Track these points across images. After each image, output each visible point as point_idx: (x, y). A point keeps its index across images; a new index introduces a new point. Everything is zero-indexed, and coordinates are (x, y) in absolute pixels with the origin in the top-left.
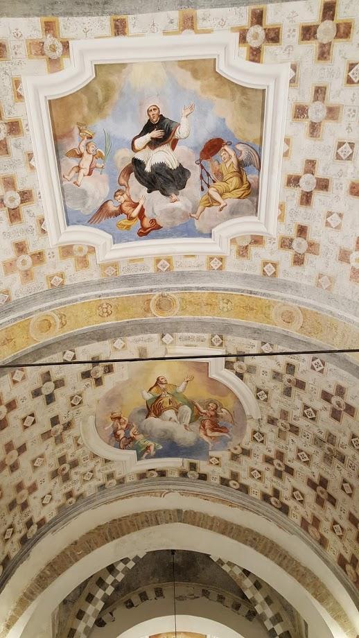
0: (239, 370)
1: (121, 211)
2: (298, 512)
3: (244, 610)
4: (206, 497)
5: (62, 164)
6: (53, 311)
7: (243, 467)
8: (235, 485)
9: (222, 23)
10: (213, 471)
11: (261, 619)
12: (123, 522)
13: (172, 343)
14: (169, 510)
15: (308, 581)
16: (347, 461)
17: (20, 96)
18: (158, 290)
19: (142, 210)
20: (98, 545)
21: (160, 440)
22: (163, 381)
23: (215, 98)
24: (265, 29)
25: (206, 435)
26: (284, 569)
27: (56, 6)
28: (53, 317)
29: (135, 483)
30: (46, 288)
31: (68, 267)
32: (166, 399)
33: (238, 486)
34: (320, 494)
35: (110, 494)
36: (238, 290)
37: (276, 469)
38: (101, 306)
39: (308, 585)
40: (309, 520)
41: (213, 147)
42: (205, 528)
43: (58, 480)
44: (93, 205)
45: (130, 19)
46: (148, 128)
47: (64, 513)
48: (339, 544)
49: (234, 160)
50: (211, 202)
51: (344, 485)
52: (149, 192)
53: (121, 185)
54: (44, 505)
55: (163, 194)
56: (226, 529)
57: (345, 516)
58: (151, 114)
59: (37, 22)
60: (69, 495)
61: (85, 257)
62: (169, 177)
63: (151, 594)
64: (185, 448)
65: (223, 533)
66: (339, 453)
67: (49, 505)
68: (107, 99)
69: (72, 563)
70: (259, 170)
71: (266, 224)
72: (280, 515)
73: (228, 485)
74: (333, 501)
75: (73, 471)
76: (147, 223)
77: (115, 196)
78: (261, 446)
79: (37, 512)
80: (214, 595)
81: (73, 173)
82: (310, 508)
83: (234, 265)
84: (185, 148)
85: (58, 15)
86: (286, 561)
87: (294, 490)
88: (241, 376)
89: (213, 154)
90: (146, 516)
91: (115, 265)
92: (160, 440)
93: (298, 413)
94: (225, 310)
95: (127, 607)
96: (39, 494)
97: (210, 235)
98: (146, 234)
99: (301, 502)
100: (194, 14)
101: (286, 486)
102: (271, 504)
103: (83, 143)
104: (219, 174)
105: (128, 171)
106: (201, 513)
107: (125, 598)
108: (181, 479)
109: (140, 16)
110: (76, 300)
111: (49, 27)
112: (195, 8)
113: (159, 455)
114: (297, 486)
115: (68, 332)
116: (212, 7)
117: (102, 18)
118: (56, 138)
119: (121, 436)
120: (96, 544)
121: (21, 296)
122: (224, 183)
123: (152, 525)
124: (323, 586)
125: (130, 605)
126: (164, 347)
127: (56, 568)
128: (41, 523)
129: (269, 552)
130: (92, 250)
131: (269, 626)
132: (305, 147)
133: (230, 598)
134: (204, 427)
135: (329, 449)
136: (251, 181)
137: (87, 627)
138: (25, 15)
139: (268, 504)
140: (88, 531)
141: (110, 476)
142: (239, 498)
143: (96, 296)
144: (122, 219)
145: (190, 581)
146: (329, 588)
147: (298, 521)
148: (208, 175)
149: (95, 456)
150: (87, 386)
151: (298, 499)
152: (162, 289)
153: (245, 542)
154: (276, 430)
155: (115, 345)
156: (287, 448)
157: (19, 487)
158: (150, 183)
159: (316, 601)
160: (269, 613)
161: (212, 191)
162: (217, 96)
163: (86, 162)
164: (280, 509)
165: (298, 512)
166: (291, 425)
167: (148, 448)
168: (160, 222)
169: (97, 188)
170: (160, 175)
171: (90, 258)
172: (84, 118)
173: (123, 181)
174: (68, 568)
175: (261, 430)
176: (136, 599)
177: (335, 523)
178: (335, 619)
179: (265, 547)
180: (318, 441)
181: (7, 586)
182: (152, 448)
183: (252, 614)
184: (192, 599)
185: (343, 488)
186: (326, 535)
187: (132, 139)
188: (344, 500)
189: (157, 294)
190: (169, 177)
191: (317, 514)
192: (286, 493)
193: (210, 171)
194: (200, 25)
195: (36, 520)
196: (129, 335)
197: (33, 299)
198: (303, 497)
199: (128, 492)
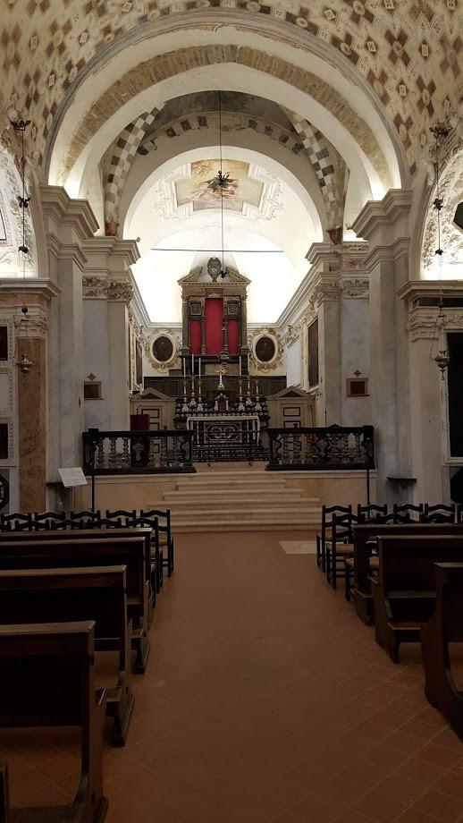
2: (368, 63)
3: (291, 142)
8: (303, 23)
11: (308, 153)
16: (434, 20)
26: (339, 120)
29: (182, 14)
33: (306, 25)
34: (395, 49)
40: (377, 74)
43: (93, 14)
47: (103, 52)
48: (400, 103)
51: (423, 46)
54: (81, 44)
56: (287, 72)
57: (414, 79)
60: (107, 30)
63: (194, 124)
67: (86, 45)
69: (118, 107)
72: (347, 63)
73: (294, 22)
74: (406, 60)
79: (76, 53)
80: (261, 126)
82: (380, 63)
86: (342, 112)
87: (369, 39)
90: (194, 53)
95: (169, 135)
96: (75, 32)
99: (374, 53)
102: (340, 50)
106: (258, 51)
107: (166, 127)
108: (238, 10)
114: (373, 36)
120: (141, 85)
124: (374, 139)
125: (171, 133)
127: (102, 111)
128: (81, 64)
129: (328, 100)
131: (314, 159)
133: (278, 130)
137: (130, 155)
139: (337, 49)
142: (304, 38)
145: (236, 110)
146: (378, 141)
147: (365, 73)
151: (371, 50)
157: (54, 28)
159: (363, 153)
160: (317, 148)
164: (349, 57)
165: (368, 63)
174: (115, 112)
176: (177, 128)
177: (402, 83)
179: (324, 96)
181: (61, 127)
183: (299, 148)
184: (238, 130)
185: (420, 49)
186: (389, 92)
188: (397, 102)
191: (386, 70)
192: (359, 41)
195: (75, 62)
198: (377, 48)
199: (175, 24)
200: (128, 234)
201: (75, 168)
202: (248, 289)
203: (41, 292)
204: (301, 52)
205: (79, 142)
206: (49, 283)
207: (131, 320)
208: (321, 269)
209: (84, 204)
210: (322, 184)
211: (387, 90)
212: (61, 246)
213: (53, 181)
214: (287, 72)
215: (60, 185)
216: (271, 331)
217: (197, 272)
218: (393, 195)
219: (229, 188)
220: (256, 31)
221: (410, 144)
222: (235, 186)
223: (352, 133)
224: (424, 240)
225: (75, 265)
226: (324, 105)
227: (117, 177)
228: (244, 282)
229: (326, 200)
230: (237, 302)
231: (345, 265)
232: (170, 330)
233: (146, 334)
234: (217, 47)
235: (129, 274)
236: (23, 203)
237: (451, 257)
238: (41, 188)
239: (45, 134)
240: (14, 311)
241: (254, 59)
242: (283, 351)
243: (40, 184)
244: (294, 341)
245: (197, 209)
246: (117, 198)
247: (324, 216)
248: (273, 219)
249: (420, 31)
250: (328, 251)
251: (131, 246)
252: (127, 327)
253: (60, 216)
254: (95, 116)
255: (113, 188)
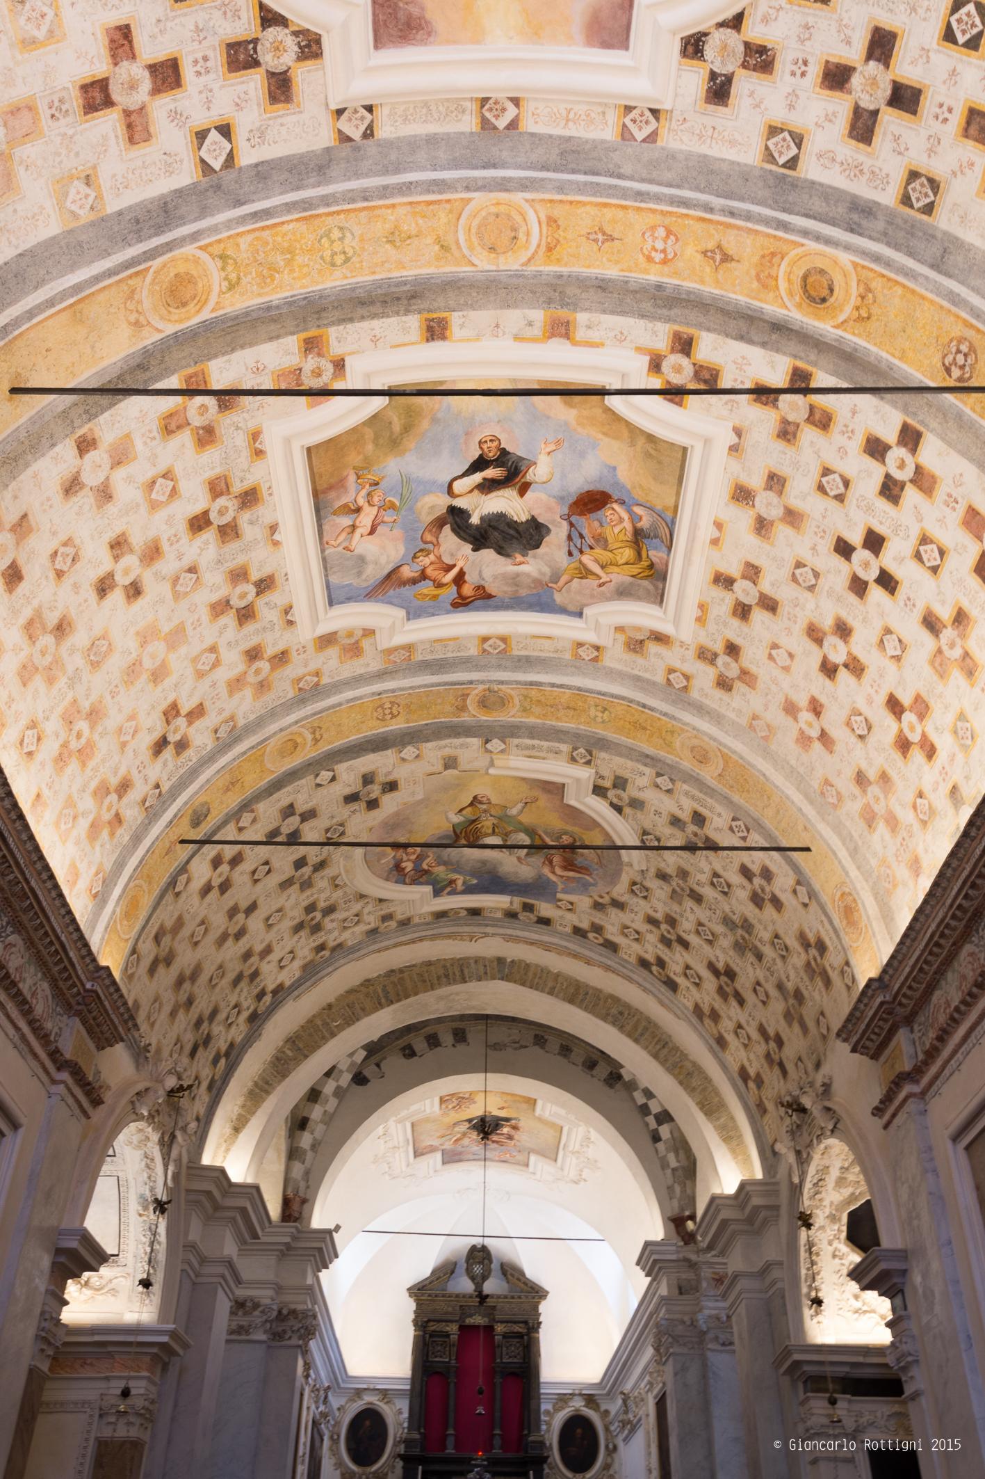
0: (615, 801)
1: (423, 576)
3: (602, 1070)
4: (547, 947)
5: (326, 527)
6: (302, 726)
7: (612, 922)
9: (621, 338)
10: (562, 917)
12: (406, 975)
13: (502, 751)
14: (484, 958)
15: (694, 1084)
17: (259, 453)
18: (482, 682)
19: (461, 574)
20: (366, 1012)
21: (473, 874)
22: (484, 800)
23: (600, 436)
24: (695, 365)
25: (553, 873)
27: (324, 314)
28: (300, 734)
29: (428, 924)
30: (291, 695)
31: (332, 665)
32: (487, 823)
33: (601, 941)
35: (386, 939)
36: (623, 698)
37: (663, 935)
38: (381, 706)
39: (694, 1089)
40: (706, 1009)
41: (592, 502)
42: (542, 991)
44: (374, 573)
45: (455, 319)
46: (479, 464)
47: (311, 972)
49: (627, 525)
50: (585, 573)
52: (474, 550)
53: (426, 543)
55: (499, 553)
56: (577, 994)
57: (754, 1024)
58: (485, 447)
59: (292, 343)
61: (357, 642)
62: (512, 532)
64: (517, 884)
65: (571, 1001)
66: (756, 947)
68: (407, 429)
69: (325, 1040)
70: (670, 548)
71: (677, 621)
75: (327, 920)
76: (467, 590)
77: (415, 557)
78: (642, 902)
81: (343, 535)
82: (708, 995)
83: (616, 656)
84: (543, 496)
85: (327, 325)
86: (665, 1051)
87: (688, 967)
88: (619, 809)
89: (591, 511)
90: (444, 967)
91: (409, 648)
92: (473, 874)
93: (704, 878)
94: (599, 719)
97: (580, 614)
98: (466, 605)
100: (571, 319)
101: (676, 960)
103: (364, 493)
104: (601, 541)
105: (439, 523)
106: (537, 966)
109: (472, 314)
110: (340, 704)
111: (311, 346)
112: (575, 311)
113: (469, 890)
115: (325, 747)
116: (604, 312)
117: (404, 318)
118: (316, 494)
119: (408, 869)
120: (363, 1009)
121: (252, 717)
122: (609, 554)
123: (455, 982)
125: (409, 1052)
126: (488, 755)
127: (301, 1045)
129: (642, 1034)
130: (369, 633)
132: (743, 545)
134: (551, 862)
135: (743, 938)
136: (654, 559)
137: (338, 1087)
138: (271, 339)
139: (646, 972)
140: (347, 988)
141: (387, 918)
143: (373, 694)
144: (426, 588)
147: (690, 1005)
148: (582, 536)
149: (362, 896)
150: (354, 812)
152: (490, 681)
153: (604, 1018)
154: (667, 889)
155: (402, 755)
156: (682, 916)
157: (247, 955)
158: (476, 539)
161: (587, 559)
162: (604, 434)
163: (365, 520)
164: (664, 983)
165: (689, 996)
166: (691, 890)
167: (452, 882)
168: (492, 588)
169: (383, 550)
170: (495, 528)
171: (366, 644)
172: (366, 458)
173: (429, 537)
174: (319, 1047)
175: (645, 883)
178: (724, 1140)
179: (635, 1027)
180: (727, 921)
182: (460, 883)
184: (516, 1049)
186: (726, 1035)
187: (449, 479)
188: (755, 1006)
189: (481, 687)
190: (512, 532)
191: (716, 1006)
193: (585, 532)
194: (580, 334)
195: (271, 987)
196: (428, 741)
197: (272, 714)
200: (319, 1219)
201: (242, 1136)
202: (543, 1308)
203: (155, 1350)
204: (598, 971)
205: (259, 1092)
206: (173, 1334)
207: (307, 1376)
208: (663, 1290)
209: (253, 1192)
210: (656, 1138)
211: (722, 1031)
212: (203, 1260)
213: (208, 1158)
214: (577, 994)
215: (218, 1164)
216: (590, 1400)
217: (445, 1271)
218: (748, 1188)
219: (505, 1130)
220: (532, 944)
221: (765, 1111)
222: (515, 1128)
223: (681, 1083)
224: (803, 1272)
225: (220, 1293)
226: (636, 1041)
227: (309, 1140)
228: (536, 1293)
229: (664, 1165)
230: (520, 1336)
231: (704, 1285)
232: (384, 1394)
233: (335, 1402)
234: (477, 960)
235: (314, 1292)
236: (160, 1207)
237: (852, 1301)
238: (188, 1168)
239: (210, 1088)
240: (102, 1384)
241: (530, 974)
242: (615, 1448)
243: (190, 1162)
244: (633, 1430)
245: (449, 1162)
246: (310, 1155)
247: (664, 1194)
248: (582, 1183)
249: (750, 970)
250: (674, 1257)
251: (324, 1240)
252: (298, 1384)
253: (210, 1210)
254: (289, 1053)
255: (306, 1140)
